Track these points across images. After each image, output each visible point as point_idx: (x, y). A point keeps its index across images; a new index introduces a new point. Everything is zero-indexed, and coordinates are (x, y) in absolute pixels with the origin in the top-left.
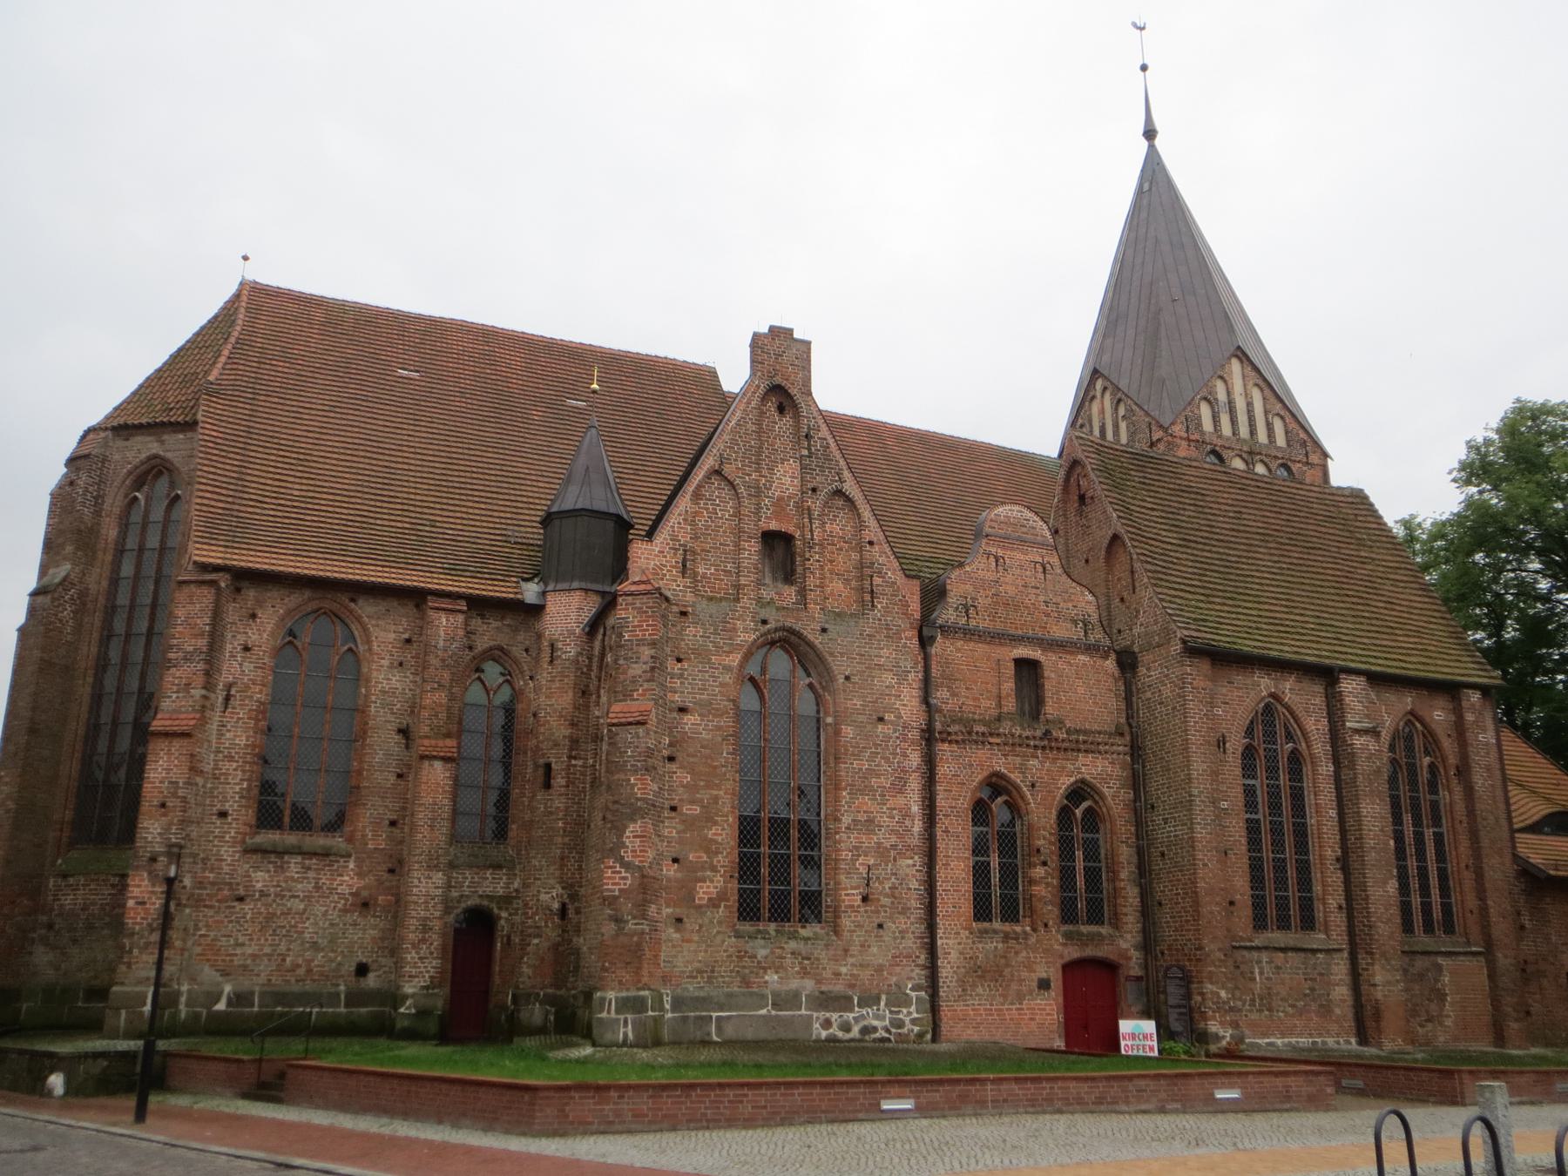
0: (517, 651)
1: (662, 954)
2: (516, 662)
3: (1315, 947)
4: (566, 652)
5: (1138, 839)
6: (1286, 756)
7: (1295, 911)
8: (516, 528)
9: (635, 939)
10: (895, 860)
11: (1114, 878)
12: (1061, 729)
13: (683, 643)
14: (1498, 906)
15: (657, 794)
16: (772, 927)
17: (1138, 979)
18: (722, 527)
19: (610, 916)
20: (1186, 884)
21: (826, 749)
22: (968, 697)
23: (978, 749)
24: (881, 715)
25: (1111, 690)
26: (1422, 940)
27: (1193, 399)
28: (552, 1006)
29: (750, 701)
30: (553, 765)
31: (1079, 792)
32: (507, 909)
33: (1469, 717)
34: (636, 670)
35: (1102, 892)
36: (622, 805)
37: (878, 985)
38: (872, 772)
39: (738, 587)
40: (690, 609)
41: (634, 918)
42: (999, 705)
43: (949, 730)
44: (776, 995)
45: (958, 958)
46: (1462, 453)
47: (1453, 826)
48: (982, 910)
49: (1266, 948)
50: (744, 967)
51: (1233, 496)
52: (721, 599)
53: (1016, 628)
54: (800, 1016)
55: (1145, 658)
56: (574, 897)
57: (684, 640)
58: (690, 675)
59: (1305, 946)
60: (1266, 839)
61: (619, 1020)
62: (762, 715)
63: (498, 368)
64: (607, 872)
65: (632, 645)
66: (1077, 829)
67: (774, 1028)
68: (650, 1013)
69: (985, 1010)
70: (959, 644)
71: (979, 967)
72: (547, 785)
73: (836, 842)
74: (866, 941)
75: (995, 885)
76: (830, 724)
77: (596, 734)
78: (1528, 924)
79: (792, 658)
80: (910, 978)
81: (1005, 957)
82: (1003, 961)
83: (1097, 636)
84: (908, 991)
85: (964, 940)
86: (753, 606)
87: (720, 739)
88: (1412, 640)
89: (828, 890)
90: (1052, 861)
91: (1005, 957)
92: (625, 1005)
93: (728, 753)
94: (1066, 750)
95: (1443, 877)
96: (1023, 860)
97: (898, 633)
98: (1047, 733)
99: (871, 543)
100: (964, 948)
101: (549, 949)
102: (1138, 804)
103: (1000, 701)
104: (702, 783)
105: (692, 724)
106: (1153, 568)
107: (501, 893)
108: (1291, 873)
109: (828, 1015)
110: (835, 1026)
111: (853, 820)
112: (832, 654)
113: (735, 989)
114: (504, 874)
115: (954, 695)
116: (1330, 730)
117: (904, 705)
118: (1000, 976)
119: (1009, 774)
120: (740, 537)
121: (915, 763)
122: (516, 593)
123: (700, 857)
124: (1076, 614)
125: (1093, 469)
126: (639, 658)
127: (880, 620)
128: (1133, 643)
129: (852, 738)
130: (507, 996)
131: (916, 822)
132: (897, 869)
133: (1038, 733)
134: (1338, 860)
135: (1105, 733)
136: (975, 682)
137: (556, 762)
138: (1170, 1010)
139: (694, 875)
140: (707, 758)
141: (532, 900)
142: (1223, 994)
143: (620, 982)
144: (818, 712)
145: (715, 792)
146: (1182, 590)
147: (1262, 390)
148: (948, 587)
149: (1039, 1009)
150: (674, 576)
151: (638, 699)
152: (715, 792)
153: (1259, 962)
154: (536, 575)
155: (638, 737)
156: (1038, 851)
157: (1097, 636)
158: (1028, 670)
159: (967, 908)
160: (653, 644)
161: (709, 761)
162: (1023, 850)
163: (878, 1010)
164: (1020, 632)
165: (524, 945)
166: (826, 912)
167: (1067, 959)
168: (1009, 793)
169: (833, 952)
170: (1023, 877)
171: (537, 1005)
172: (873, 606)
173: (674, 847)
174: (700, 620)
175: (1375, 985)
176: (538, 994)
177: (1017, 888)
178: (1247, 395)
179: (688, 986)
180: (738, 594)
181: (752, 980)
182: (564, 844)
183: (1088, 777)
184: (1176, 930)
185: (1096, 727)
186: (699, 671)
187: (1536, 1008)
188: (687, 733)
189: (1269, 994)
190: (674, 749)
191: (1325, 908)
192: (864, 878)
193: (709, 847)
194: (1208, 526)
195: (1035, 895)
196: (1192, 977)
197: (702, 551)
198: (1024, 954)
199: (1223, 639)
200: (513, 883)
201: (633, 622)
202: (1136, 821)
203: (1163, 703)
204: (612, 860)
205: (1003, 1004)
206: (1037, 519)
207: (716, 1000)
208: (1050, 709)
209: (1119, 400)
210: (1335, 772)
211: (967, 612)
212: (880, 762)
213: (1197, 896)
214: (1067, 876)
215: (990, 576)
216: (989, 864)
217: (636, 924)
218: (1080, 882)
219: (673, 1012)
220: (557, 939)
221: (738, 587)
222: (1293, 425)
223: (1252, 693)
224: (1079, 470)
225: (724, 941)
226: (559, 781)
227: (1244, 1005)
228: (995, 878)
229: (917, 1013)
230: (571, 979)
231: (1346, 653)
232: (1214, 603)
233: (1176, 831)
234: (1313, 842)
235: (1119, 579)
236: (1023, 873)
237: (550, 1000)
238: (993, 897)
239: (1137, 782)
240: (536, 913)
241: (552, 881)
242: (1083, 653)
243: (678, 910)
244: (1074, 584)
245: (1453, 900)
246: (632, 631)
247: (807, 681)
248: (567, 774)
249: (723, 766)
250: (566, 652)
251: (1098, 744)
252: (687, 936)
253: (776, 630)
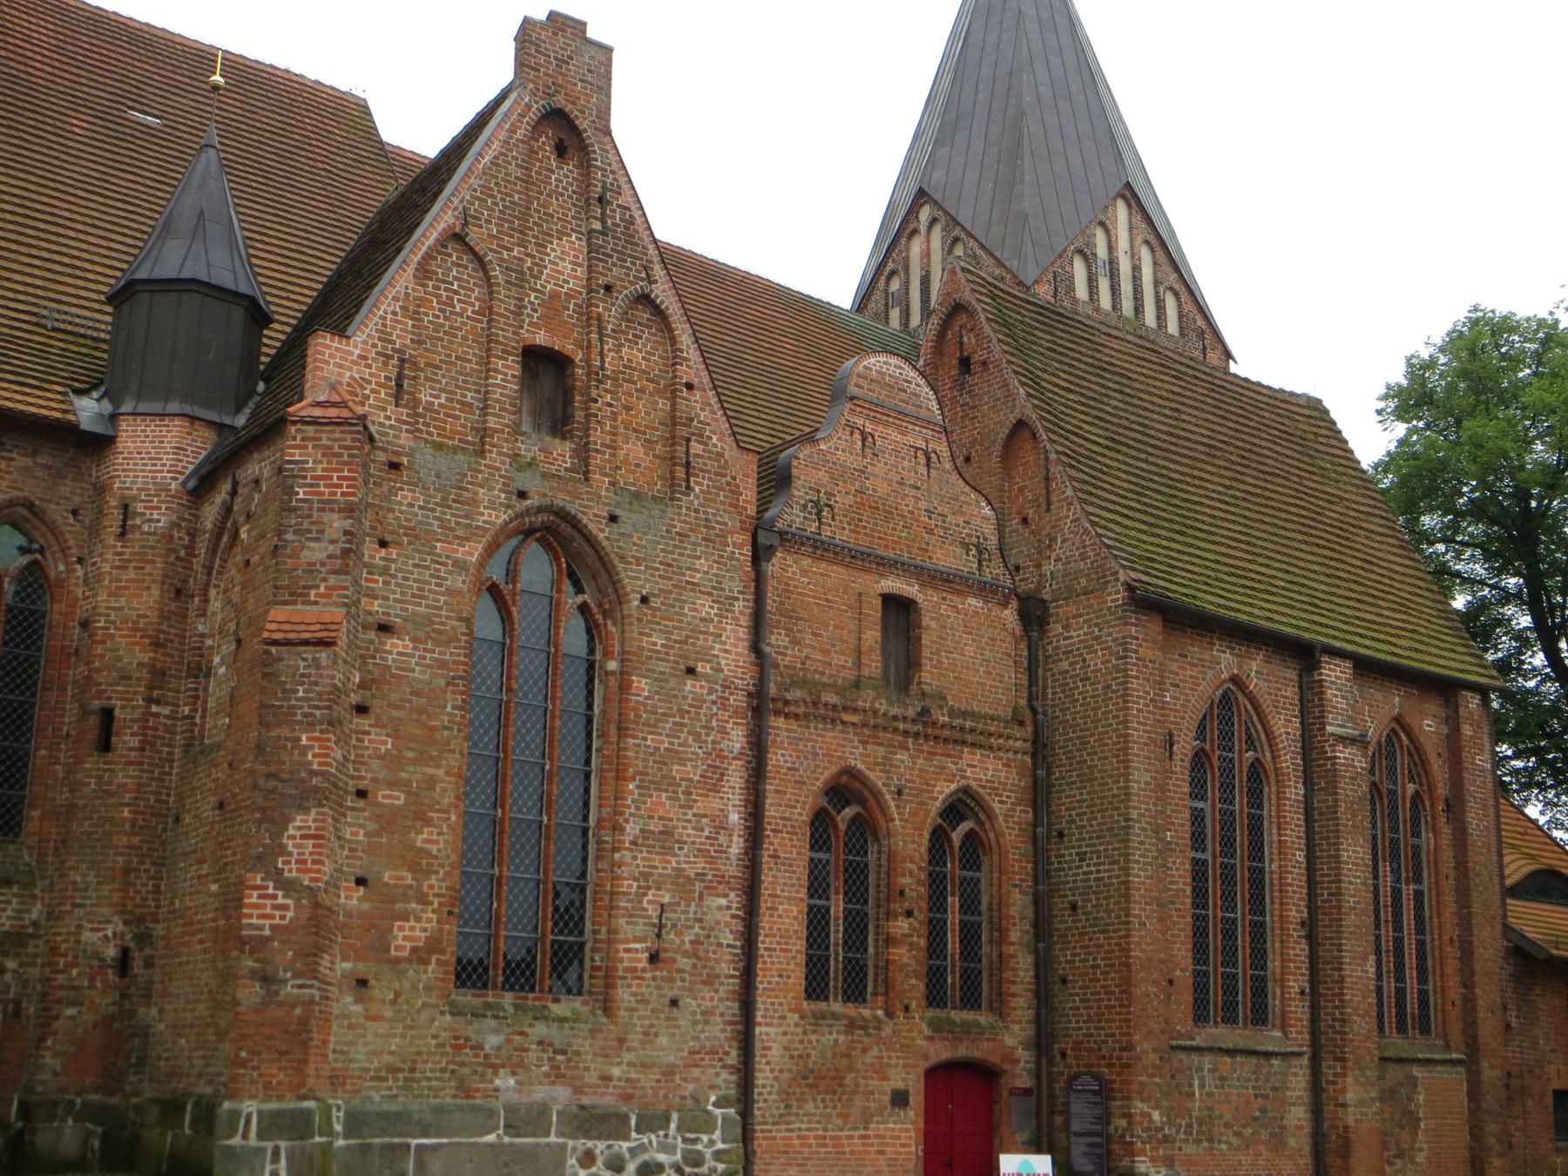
0: (57, 512)
1: (332, 1039)
2: (54, 531)
3: (1270, 1048)
4: (150, 521)
5: (1036, 881)
6: (1245, 770)
7: (1244, 996)
8: (54, 305)
9: (298, 1011)
10: (701, 897)
11: (1001, 939)
12: (941, 707)
13: (391, 515)
14: (1488, 993)
15: (342, 766)
16: (508, 999)
17: (1027, 1092)
18: (460, 329)
19: (253, 971)
20: (1112, 951)
21: (604, 712)
22: (814, 648)
23: (825, 729)
24: (691, 664)
25: (1009, 655)
26: (1398, 1045)
27: (1065, 250)
28: (98, 1124)
29: (488, 625)
30: (117, 712)
31: (961, 806)
32: (17, 955)
33: (1467, 731)
34: (316, 552)
35: (980, 960)
36: (282, 781)
37: (665, 1097)
38: (675, 755)
39: (483, 433)
40: (405, 460)
41: (296, 975)
42: (859, 666)
43: (788, 696)
44: (511, 1110)
45: (782, 1056)
46: (1399, 376)
47: (1437, 882)
48: (816, 986)
49: (1210, 1049)
50: (463, 1064)
51: (1166, 386)
52: (455, 450)
53: (886, 546)
54: (548, 1145)
55: (1061, 611)
56: (143, 939)
57: (393, 511)
58: (400, 570)
59: (1259, 1048)
60: (1213, 887)
61: (263, 1150)
62: (506, 651)
63: (10, 40)
64: (250, 896)
65: (310, 509)
66: (953, 862)
67: (506, 1165)
68: (318, 1139)
69: (816, 1137)
70: (806, 562)
71: (812, 1071)
72: (105, 746)
73: (613, 864)
74: (653, 1026)
75: (836, 945)
76: (613, 673)
77: (199, 663)
78: (1514, 1022)
79: (557, 559)
80: (712, 1087)
81: (848, 1056)
82: (845, 1062)
83: (994, 571)
84: (710, 1108)
85: (792, 1029)
86: (505, 466)
87: (442, 682)
88: (1398, 616)
89: (596, 941)
90: (920, 910)
91: (848, 1056)
92: (273, 1125)
93: (454, 707)
94: (946, 740)
95: (1421, 955)
96: (878, 906)
97: (722, 535)
98: (925, 712)
99: (689, 386)
100: (792, 1041)
101: (95, 1026)
102: (1039, 830)
103: (859, 658)
104: (411, 755)
105: (399, 654)
106: (1080, 475)
107: (7, 928)
108: (1243, 939)
109: (590, 1144)
110: (600, 1162)
111: (643, 831)
112: (622, 558)
113: (449, 1100)
114: (14, 895)
115: (795, 642)
116: (1303, 736)
117: (726, 651)
118: (840, 1085)
119: (867, 772)
120: (489, 349)
121: (738, 746)
122: (66, 411)
123: (402, 878)
124: (970, 535)
125: (988, 319)
126: (322, 532)
127: (697, 511)
128: (1040, 586)
129: (647, 698)
130: (10, 1105)
131: (735, 839)
132: (705, 913)
133: (911, 712)
134: (1303, 924)
135: (998, 718)
136: (826, 624)
137: (123, 707)
138: (1073, 1139)
139: (389, 908)
140: (420, 713)
141: (67, 941)
142: (1156, 1116)
143: (267, 1086)
144: (591, 651)
145: (431, 771)
146: (1118, 513)
147: (1153, 251)
148: (795, 472)
149: (892, 1137)
150: (383, 401)
151: (316, 603)
152: (431, 771)
153: (1200, 1070)
154: (95, 387)
155: (319, 667)
156: (902, 893)
157: (994, 571)
158: (898, 609)
159: (797, 979)
160: (349, 510)
161: (424, 717)
162: (878, 892)
163: (666, 1136)
164: (891, 554)
165: (46, 1020)
166: (591, 977)
167: (933, 1061)
168: (862, 802)
169: (601, 1043)
170: (877, 933)
171: (70, 1122)
172: (688, 487)
173: (360, 859)
174: (420, 479)
175: (1345, 1105)
176: (71, 1104)
177: (866, 950)
178: (1134, 254)
179: (373, 1093)
180: (483, 444)
181: (475, 1085)
182: (130, 847)
183: (974, 784)
184: (1090, 1020)
185: (986, 710)
186: (416, 566)
187: (1518, 1138)
188: (388, 667)
189: (1210, 1117)
190: (368, 693)
191: (1283, 993)
192: (654, 925)
193: (417, 863)
194: (1140, 424)
195: (895, 962)
196: (1112, 1090)
197: (428, 364)
198: (875, 1051)
199: (1179, 590)
200: (29, 911)
201: (314, 470)
202: (1035, 855)
203: (1088, 679)
204: (259, 876)
205: (841, 1130)
206: (922, 382)
207: (416, 1117)
208: (928, 676)
209: (956, 240)
210: (1305, 796)
211: (819, 514)
212: (686, 739)
213: (1129, 971)
214: (936, 931)
215: (853, 461)
216: (828, 911)
217: (300, 987)
218: (953, 943)
219: (346, 1136)
220: (113, 1009)
221: (483, 433)
222: (1189, 307)
223: (1210, 673)
224: (962, 318)
225: (433, 1020)
226: (126, 740)
227: (1178, 1133)
228: (837, 932)
229: (724, 1141)
230: (133, 1079)
231: (1327, 626)
232: (1159, 536)
233: (1098, 872)
234: (1272, 898)
235: (1022, 489)
236: (877, 926)
237: (92, 1113)
238: (832, 963)
239: (1039, 795)
240: (74, 964)
241: (106, 911)
242: (975, 595)
243: (361, 965)
244: (967, 489)
245: (1431, 987)
246: (311, 485)
247: (580, 599)
248: (144, 728)
249: (445, 728)
250: (150, 521)
251: (990, 735)
252: (374, 1009)
253: (540, 510)
